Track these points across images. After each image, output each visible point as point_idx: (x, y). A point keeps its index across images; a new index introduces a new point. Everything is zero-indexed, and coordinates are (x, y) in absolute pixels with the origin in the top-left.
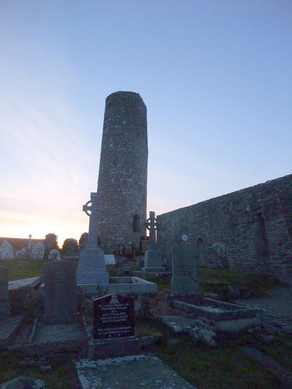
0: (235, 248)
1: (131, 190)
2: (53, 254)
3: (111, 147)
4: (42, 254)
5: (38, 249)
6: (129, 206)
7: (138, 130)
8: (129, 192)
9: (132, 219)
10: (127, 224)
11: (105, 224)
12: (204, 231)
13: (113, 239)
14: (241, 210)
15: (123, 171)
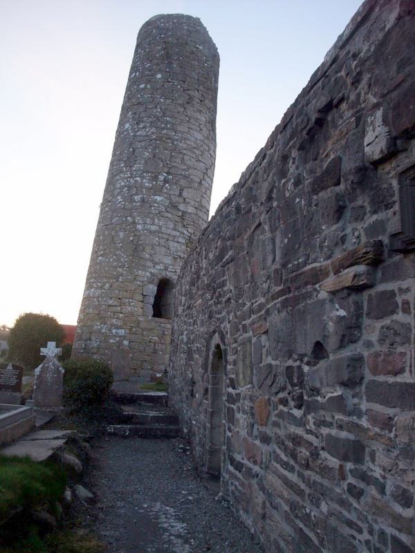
3: (127, 130)
8: (153, 224)
10: (141, 298)
13: (104, 331)
15: (143, 178)
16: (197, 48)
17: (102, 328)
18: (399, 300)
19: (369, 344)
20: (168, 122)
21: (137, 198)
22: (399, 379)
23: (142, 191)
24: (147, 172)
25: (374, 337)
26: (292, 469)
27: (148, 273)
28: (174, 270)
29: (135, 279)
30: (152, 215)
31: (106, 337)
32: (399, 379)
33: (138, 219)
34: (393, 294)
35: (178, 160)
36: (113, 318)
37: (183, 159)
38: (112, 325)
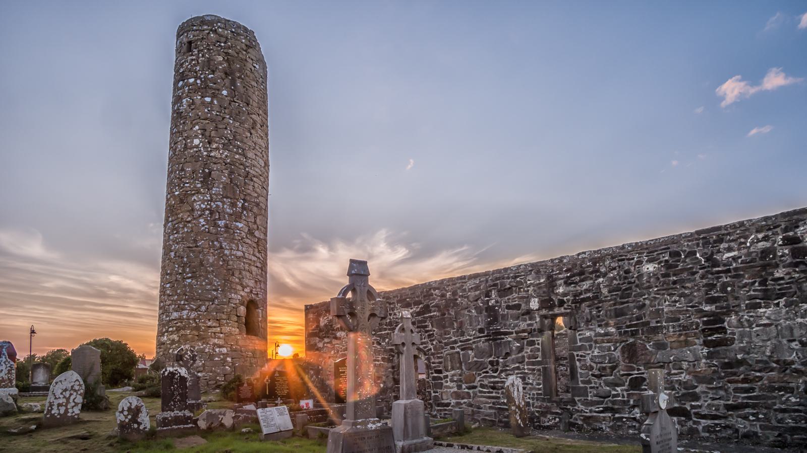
0: (497, 379)
1: (240, 247)
2: (129, 409)
3: (197, 146)
4: (76, 404)
5: (66, 390)
6: (237, 280)
7: (253, 116)
8: (238, 250)
9: (242, 310)
10: (235, 318)
11: (188, 319)
12: (424, 343)
13: (207, 350)
14: (518, 307)
15: (224, 203)
16: (255, 67)
17: (205, 348)
18: (537, 342)
19: (527, 352)
20: (238, 147)
21: (221, 223)
22: (537, 360)
23: (224, 217)
24: (227, 197)
25: (529, 351)
26: (492, 393)
27: (239, 296)
28: (256, 293)
29: (229, 302)
30: (236, 241)
31: (211, 357)
32: (537, 360)
33: (224, 244)
34: (534, 341)
35: (251, 188)
36: (215, 338)
37: (254, 186)
38: (215, 344)
